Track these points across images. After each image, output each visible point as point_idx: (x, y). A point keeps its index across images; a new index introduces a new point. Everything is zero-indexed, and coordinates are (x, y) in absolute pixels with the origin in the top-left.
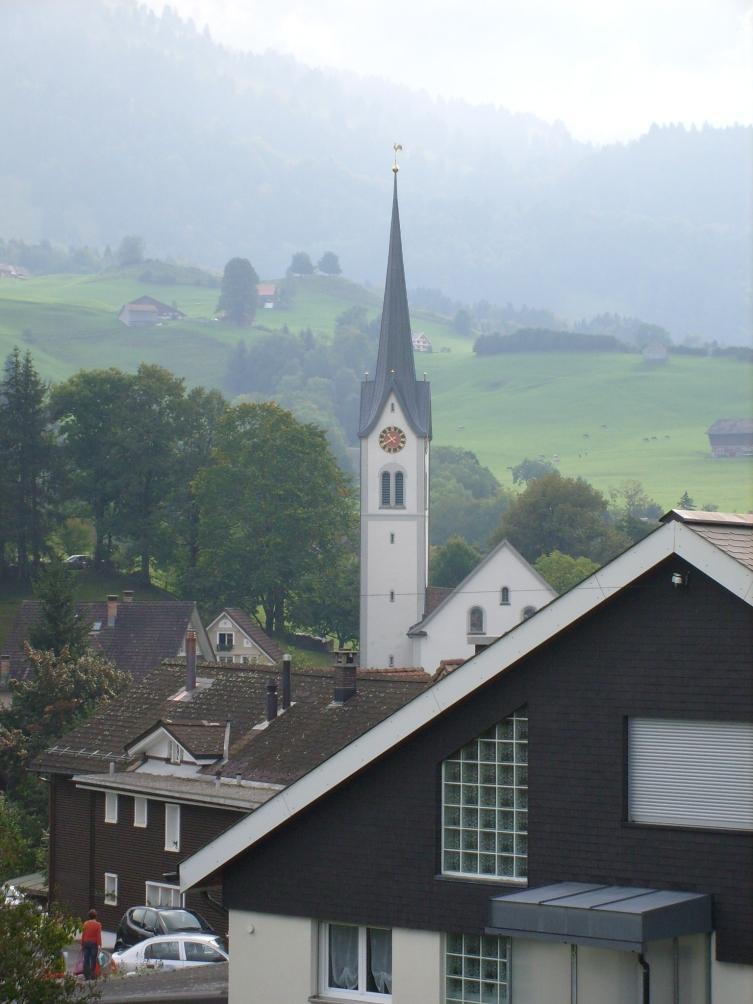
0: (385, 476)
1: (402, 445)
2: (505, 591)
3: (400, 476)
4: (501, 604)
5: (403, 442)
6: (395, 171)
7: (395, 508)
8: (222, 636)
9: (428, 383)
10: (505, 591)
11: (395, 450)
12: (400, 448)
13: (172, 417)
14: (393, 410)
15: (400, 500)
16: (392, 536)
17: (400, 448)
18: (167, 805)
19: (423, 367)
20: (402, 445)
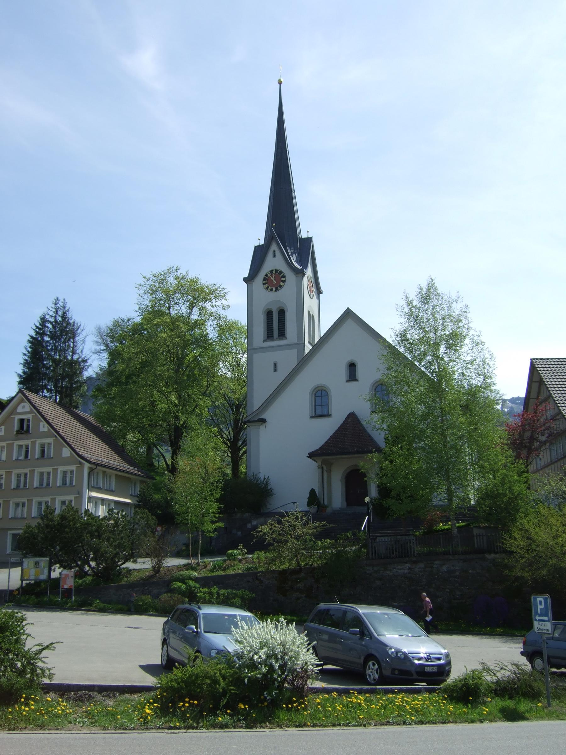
0: (269, 314)
1: (282, 284)
2: (352, 366)
3: (282, 313)
4: (347, 381)
5: (284, 281)
6: (280, 83)
7: (277, 339)
8: (22, 421)
9: (311, 238)
10: (352, 366)
11: (277, 289)
12: (281, 286)
13: (55, 549)
14: (274, 256)
15: (282, 334)
16: (275, 365)
17: (281, 286)
18: (20, 568)
19: (305, 229)
20: (282, 284)
